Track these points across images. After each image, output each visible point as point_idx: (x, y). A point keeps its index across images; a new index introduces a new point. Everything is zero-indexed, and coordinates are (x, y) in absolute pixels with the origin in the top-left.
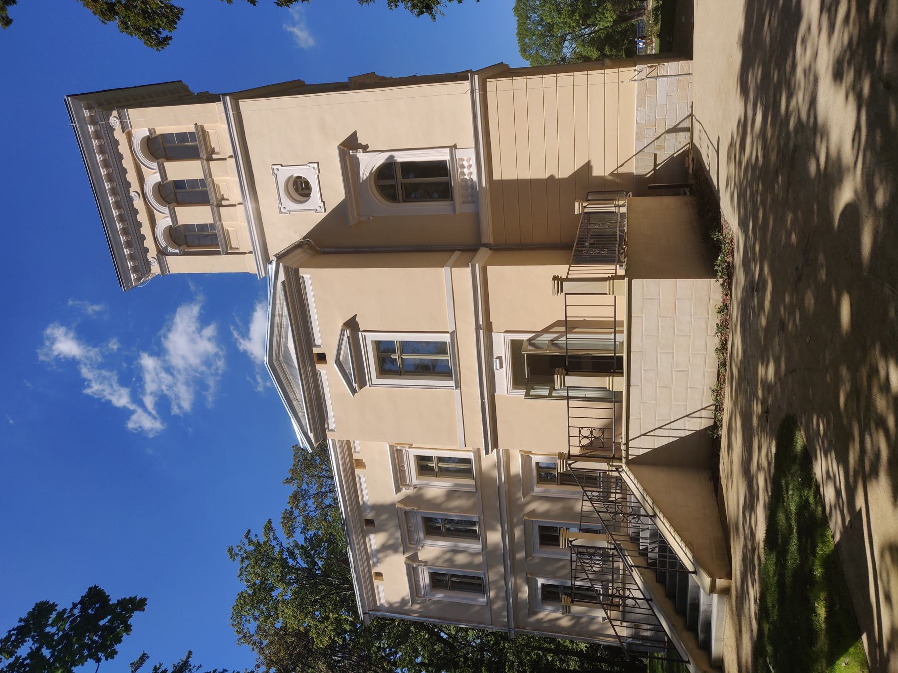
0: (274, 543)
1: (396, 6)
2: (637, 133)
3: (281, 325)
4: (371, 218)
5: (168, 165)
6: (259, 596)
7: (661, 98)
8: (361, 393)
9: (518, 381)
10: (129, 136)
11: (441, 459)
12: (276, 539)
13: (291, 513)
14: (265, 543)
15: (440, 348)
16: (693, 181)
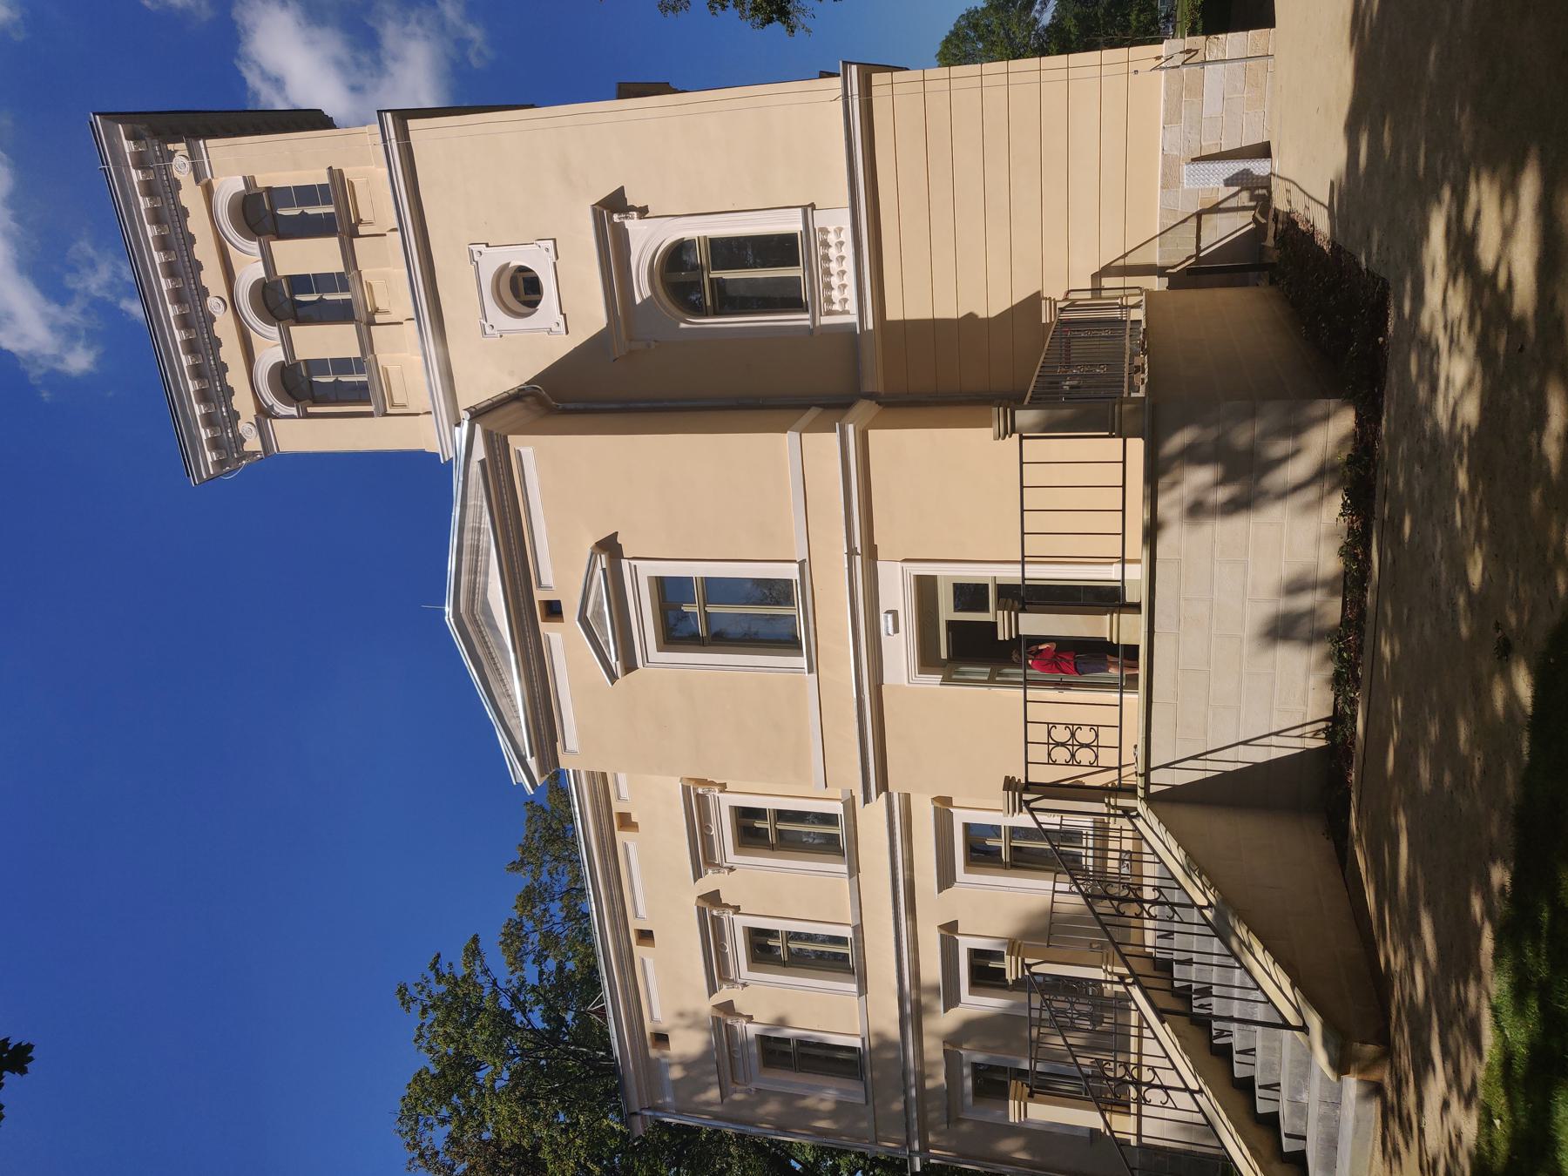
0: (482, 979)
1: (724, 7)
2: (1164, 175)
3: (476, 550)
4: (653, 345)
5: (278, 247)
6: (452, 1080)
7: (1212, 104)
8: (622, 680)
9: (928, 660)
10: (208, 191)
11: (782, 815)
12: (486, 972)
13: (519, 925)
14: (464, 979)
15: (777, 592)
16: (1274, 256)
